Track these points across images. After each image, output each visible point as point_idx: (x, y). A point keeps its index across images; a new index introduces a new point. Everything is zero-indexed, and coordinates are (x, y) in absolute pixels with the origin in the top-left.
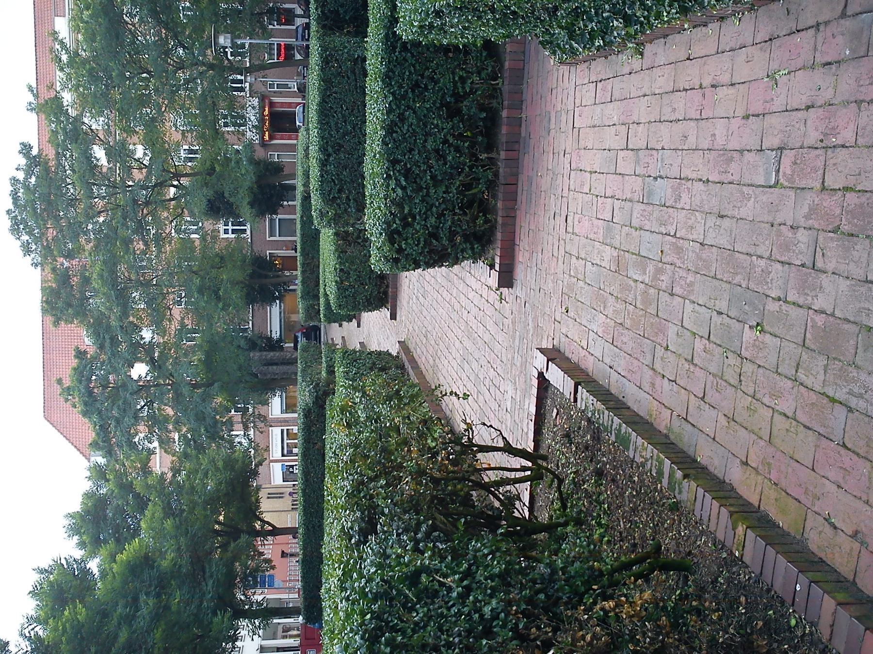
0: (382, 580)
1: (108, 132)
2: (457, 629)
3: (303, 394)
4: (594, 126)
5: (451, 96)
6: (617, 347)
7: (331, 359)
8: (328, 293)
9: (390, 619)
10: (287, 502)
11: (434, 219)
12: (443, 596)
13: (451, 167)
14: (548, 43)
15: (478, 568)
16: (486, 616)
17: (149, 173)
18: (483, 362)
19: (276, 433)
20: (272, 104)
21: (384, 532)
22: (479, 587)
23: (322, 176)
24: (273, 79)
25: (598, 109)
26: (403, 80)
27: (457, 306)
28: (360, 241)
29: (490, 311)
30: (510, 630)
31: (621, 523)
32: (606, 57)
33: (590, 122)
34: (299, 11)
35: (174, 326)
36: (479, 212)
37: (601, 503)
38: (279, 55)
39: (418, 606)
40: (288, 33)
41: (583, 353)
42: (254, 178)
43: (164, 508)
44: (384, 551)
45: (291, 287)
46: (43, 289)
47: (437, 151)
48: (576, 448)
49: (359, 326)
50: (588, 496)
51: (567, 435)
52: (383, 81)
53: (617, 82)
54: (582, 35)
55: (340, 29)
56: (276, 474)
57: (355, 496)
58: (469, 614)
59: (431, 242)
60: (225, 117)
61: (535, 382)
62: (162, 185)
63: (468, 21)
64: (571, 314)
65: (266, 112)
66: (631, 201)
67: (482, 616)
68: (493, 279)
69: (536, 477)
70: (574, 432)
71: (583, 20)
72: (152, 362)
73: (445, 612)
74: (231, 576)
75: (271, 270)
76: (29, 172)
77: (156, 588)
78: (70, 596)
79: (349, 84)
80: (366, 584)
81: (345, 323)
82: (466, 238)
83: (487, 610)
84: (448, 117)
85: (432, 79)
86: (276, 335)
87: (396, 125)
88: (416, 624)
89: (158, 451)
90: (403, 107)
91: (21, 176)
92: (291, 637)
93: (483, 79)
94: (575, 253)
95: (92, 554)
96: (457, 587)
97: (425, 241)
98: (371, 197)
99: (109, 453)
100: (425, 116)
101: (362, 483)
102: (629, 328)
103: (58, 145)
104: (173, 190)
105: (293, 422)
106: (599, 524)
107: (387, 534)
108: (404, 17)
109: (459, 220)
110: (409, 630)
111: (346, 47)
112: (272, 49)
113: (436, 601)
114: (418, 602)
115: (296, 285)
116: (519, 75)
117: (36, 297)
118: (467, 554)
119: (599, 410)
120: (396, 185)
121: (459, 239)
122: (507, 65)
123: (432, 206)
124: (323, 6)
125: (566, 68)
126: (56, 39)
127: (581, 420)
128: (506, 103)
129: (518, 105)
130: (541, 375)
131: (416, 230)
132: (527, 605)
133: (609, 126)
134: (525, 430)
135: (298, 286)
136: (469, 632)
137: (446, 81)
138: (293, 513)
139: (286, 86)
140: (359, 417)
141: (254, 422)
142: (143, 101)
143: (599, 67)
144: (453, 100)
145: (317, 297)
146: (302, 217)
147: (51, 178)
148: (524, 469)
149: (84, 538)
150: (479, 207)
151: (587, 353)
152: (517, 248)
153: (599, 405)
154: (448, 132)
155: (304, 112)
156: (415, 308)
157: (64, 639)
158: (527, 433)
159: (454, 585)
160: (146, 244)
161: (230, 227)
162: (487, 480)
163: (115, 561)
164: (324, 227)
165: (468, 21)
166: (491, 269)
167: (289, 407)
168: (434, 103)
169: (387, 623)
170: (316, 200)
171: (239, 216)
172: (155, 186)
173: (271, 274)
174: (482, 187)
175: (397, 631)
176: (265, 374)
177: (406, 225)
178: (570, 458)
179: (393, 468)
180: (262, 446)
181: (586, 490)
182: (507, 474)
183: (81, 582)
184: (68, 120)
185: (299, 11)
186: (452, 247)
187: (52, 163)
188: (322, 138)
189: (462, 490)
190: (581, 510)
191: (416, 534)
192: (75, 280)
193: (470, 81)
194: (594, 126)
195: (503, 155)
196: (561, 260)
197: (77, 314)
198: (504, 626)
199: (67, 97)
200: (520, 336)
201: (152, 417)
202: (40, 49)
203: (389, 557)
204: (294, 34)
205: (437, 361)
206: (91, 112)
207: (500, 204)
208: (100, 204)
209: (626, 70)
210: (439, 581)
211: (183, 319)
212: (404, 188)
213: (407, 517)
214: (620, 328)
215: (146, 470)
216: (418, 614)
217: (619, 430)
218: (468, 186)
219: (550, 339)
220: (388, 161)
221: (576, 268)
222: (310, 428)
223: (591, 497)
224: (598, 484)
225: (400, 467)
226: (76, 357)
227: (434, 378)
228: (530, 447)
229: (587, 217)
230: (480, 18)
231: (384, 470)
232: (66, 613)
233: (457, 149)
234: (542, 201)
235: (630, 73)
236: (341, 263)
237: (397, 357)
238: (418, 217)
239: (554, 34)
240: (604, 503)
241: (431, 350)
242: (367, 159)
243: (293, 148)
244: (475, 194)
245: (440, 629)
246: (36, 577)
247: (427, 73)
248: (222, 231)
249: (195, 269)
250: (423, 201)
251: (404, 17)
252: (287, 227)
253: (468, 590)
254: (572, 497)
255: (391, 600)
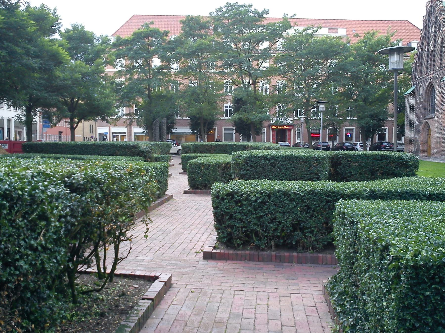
0: (43, 199)
1: (275, 50)
2: (10, 246)
3: (144, 144)
4: (292, 306)
5: (304, 226)
6: (174, 322)
7: (163, 159)
8: (198, 159)
9: (18, 205)
10: (88, 135)
11: (240, 217)
12: (32, 235)
13: (267, 226)
14: (336, 279)
15: (49, 254)
16: (17, 263)
17: (256, 70)
18: (163, 242)
19: (124, 130)
20: (289, 130)
21: (71, 198)
22: (36, 256)
23: (259, 157)
24: (302, 130)
25: (301, 308)
26: (311, 201)
27: (192, 227)
28: (224, 175)
29: (190, 246)
30: (7, 279)
31: (73, 330)
32: (329, 312)
33: (294, 303)
34: (335, 143)
35: (180, 80)
36: (243, 241)
37: (85, 316)
38: (314, 134)
39: (26, 221)
40: (324, 138)
41: (169, 302)
42: (254, 120)
43: (86, 73)
44: (61, 198)
45: (199, 138)
46: (198, 16)
47: (275, 218)
48: (117, 300)
49: (180, 173)
50: (90, 308)
51: (124, 294)
52: (311, 190)
53: (316, 319)
54: (342, 300)
55: (332, 166)
56: (103, 129)
57: (92, 180)
58: (19, 252)
59: (227, 215)
60: (283, 107)
61: (153, 274)
62: (250, 75)
63: (348, 239)
64: (191, 294)
65: (285, 127)
66: (254, 329)
67: (18, 260)
68: (208, 249)
69: (100, 275)
70: (126, 298)
71: (350, 301)
72: (161, 68)
73: (21, 238)
74: (49, 106)
75: (207, 128)
76: (256, 13)
77: (44, 67)
78: (41, 23)
79: (305, 171)
80: (41, 190)
81: (181, 166)
82: (230, 234)
83: (22, 263)
84: (293, 224)
85: (312, 216)
86: (175, 131)
87: (288, 197)
88: (14, 221)
89: (116, 70)
90: (297, 201)
91: (253, 9)
92: (16, 136)
93: (312, 242)
94: (224, 296)
95: (62, 35)
96: (37, 243)
97: (228, 212)
98: (250, 184)
99: (115, 45)
100: (293, 212)
101: (100, 184)
102: (185, 330)
103: (268, 26)
104: (247, 81)
105: (130, 139)
106: (73, 316)
107: (70, 199)
108: (348, 204)
109: (239, 230)
110: (10, 217)
111: (324, 169)
112: (316, 130)
113: (29, 232)
114: (29, 221)
115: (200, 141)
116: (315, 261)
117: (194, 13)
118: (57, 247)
119: (138, 313)
120: (258, 197)
121: (229, 230)
122: (320, 255)
123: (246, 216)
124: (343, 158)
125: (321, 288)
126: (318, 28)
127: (132, 302)
128: (300, 255)
129: (300, 261)
130: (156, 278)
131: (234, 207)
132: (23, 287)
133: (293, 315)
134: (126, 268)
135: (200, 142)
136: (8, 253)
137: (311, 223)
138: (82, 138)
139: (298, 137)
140: (135, 179)
141: (130, 118)
142: (290, 67)
143: (323, 308)
144: (301, 227)
145: (194, 152)
146: (235, 145)
147: (252, 22)
148: (105, 268)
149: (72, 32)
150: (246, 241)
151: (169, 304)
152: (225, 261)
153: (141, 314)
154: (285, 225)
155: (286, 146)
156: (190, 204)
157: (18, 19)
158: (124, 269)
159: (38, 241)
160: (220, 67)
161: (229, 109)
162: (99, 249)
163: (59, 46)
164: (233, 158)
165: (348, 239)
166: (213, 247)
167: (138, 137)
168: (300, 217)
169: (16, 204)
170: (246, 153)
171: (234, 113)
172: (249, 72)
173: (206, 129)
174: (257, 242)
175: (10, 210)
176: (155, 125)
177: (236, 202)
178: (111, 296)
179: (107, 200)
180: (118, 123)
181: (93, 306)
182: (102, 261)
183: (48, 30)
184: (281, 31)
185: (335, 143)
186: (225, 227)
187: (259, 23)
188: (278, 157)
189: (94, 236)
190: (81, 304)
191: (70, 216)
192: (203, 32)
193: (311, 235)
194: (292, 306)
195: (274, 253)
196: (220, 288)
197: (186, 32)
198: (10, 274)
199: (291, 32)
200: (177, 264)
201: (133, 68)
202: (313, 21)
203: (57, 200)
204: (324, 141)
205: (163, 216)
206: (285, 42)
207: (247, 252)
208: (240, 45)
209: (324, 325)
210: (41, 232)
211: (183, 84)
212: (256, 201)
213: (80, 210)
214: (184, 324)
215: (106, 63)
216: (21, 221)
217: (127, 327)
218: (257, 234)
219: (177, 282)
220: (270, 193)
221: (216, 297)
222: (127, 148)
223: (89, 309)
224: (96, 314)
225: (108, 204)
226: (165, 31)
227: (154, 214)
228: (117, 272)
229: (243, 303)
230: (350, 245)
231: (106, 195)
232: (32, 22)
233: (276, 229)
234: (250, 276)
235: (323, 327)
236: (213, 165)
237: (164, 194)
238: (241, 208)
239: (341, 284)
240: (85, 318)
241: (168, 213)
242: (270, 181)
243: (268, 140)
244: (252, 238)
245: (11, 235)
246: (52, 9)
247: (315, 213)
248: (227, 105)
249: (208, 91)
250: (249, 211)
251: (348, 204)
252: (229, 137)
253: (35, 250)
254: (89, 298)
255: (31, 205)
